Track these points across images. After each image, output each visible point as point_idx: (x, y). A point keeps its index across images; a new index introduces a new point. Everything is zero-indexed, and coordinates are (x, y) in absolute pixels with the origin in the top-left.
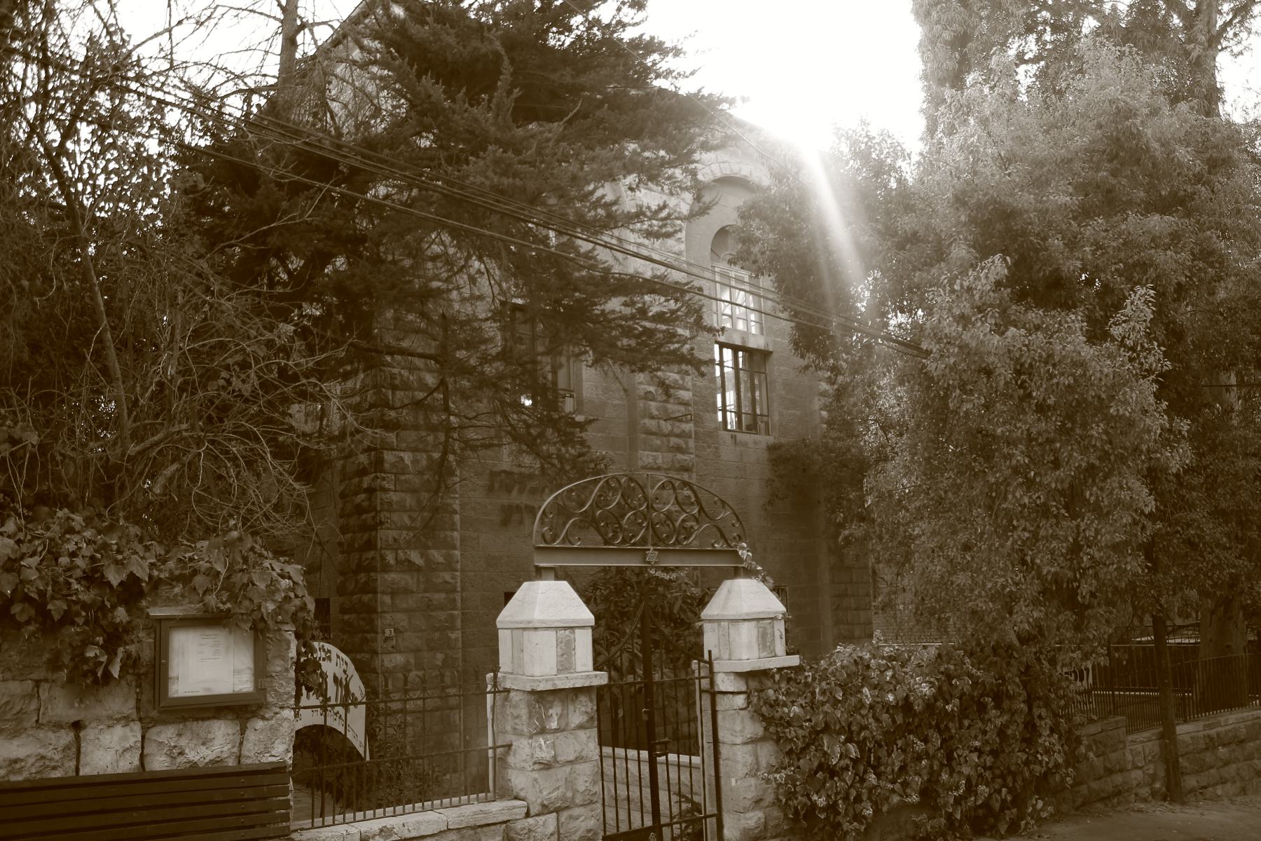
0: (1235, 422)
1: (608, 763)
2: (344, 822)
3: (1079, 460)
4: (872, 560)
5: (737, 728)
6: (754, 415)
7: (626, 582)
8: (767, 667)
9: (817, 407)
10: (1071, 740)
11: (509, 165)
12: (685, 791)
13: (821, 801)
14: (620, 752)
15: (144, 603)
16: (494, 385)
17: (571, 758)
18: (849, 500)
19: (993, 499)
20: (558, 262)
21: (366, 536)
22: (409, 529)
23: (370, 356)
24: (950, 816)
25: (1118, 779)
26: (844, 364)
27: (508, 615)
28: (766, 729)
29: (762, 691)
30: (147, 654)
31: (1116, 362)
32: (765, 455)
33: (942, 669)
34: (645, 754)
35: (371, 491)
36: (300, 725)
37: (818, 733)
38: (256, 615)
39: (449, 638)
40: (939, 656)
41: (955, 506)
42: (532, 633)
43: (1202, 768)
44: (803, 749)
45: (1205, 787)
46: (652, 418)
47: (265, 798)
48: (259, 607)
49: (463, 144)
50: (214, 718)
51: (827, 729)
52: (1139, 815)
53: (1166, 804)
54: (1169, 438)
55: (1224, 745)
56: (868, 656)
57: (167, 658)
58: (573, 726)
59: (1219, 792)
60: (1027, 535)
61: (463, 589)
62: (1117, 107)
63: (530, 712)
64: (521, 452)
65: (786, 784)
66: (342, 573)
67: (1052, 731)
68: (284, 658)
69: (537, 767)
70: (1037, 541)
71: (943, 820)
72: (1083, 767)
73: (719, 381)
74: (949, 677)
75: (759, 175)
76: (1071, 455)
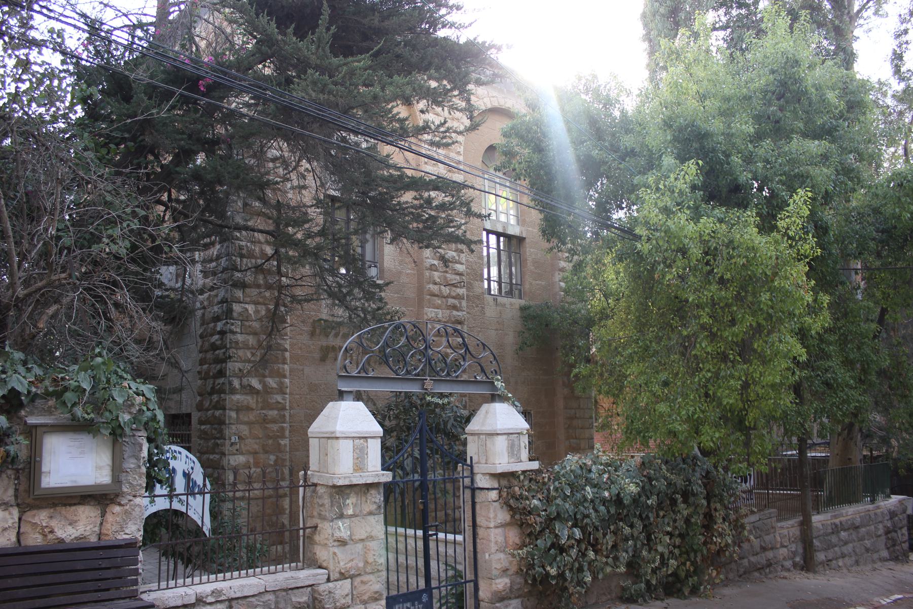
0: (859, 297)
1: (392, 540)
2: (184, 585)
3: (750, 320)
4: (594, 393)
5: (493, 517)
6: (511, 283)
7: (413, 405)
8: (514, 470)
9: (557, 280)
10: (738, 527)
11: (325, 85)
12: (451, 561)
13: (553, 571)
14: (401, 530)
15: (23, 413)
16: (316, 255)
17: (363, 537)
18: (579, 347)
19: (686, 348)
20: (367, 163)
21: (218, 367)
22: (249, 361)
23: (223, 231)
24: (648, 583)
25: (770, 554)
26: (579, 248)
27: (317, 427)
28: (512, 517)
29: (510, 488)
30: (23, 454)
31: (777, 250)
32: (519, 314)
33: (645, 473)
34: (420, 533)
35: (222, 333)
36: (153, 509)
37: (551, 520)
38: (114, 424)
39: (280, 444)
40: (643, 463)
41: (658, 353)
42: (334, 441)
43: (829, 546)
44: (540, 532)
45: (830, 560)
46: (435, 284)
47: (119, 567)
48: (118, 417)
49: (291, 66)
50: (79, 504)
51: (558, 517)
52: (785, 581)
53: (803, 573)
54: (813, 309)
55: (845, 530)
56: (590, 463)
57: (41, 456)
58: (365, 512)
59: (840, 564)
60: (709, 375)
61: (291, 408)
62: (787, 58)
63: (332, 502)
64: (334, 305)
65: (527, 558)
66: (200, 394)
67: (724, 520)
68: (138, 459)
69: (336, 544)
70: (718, 379)
71: (643, 585)
72: (745, 546)
73: (486, 259)
74: (650, 479)
75: (516, 104)
76: (744, 317)
